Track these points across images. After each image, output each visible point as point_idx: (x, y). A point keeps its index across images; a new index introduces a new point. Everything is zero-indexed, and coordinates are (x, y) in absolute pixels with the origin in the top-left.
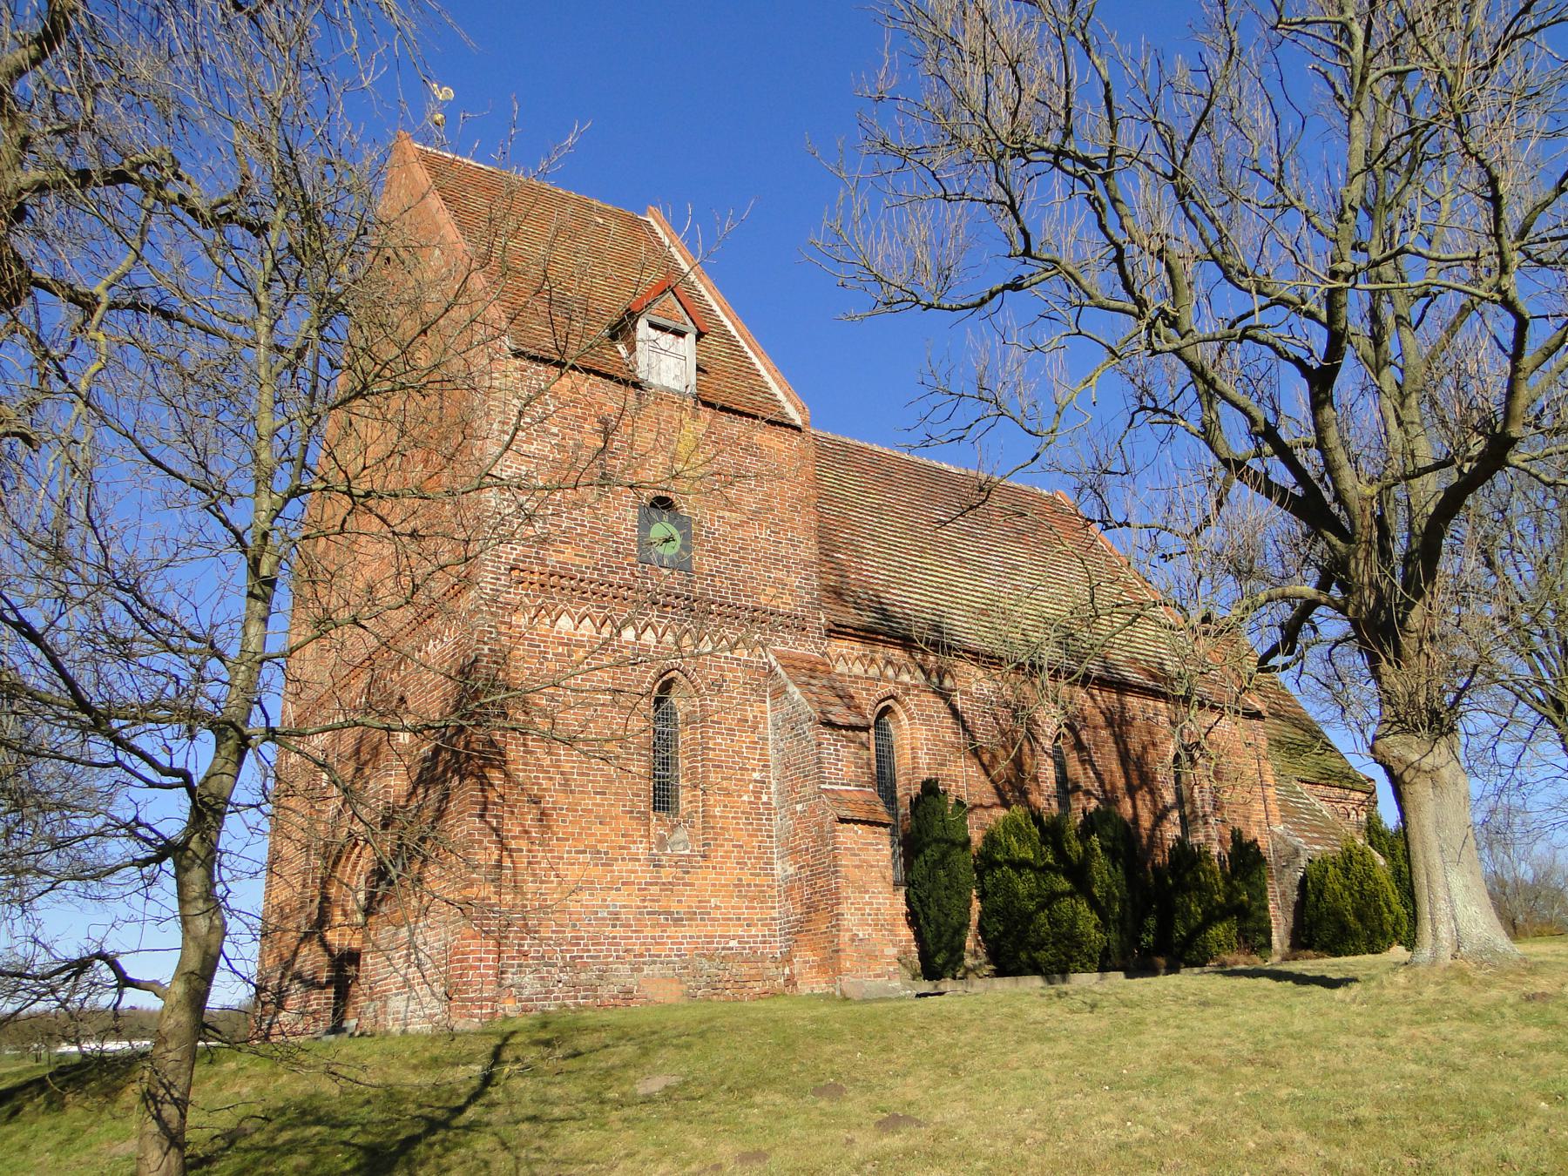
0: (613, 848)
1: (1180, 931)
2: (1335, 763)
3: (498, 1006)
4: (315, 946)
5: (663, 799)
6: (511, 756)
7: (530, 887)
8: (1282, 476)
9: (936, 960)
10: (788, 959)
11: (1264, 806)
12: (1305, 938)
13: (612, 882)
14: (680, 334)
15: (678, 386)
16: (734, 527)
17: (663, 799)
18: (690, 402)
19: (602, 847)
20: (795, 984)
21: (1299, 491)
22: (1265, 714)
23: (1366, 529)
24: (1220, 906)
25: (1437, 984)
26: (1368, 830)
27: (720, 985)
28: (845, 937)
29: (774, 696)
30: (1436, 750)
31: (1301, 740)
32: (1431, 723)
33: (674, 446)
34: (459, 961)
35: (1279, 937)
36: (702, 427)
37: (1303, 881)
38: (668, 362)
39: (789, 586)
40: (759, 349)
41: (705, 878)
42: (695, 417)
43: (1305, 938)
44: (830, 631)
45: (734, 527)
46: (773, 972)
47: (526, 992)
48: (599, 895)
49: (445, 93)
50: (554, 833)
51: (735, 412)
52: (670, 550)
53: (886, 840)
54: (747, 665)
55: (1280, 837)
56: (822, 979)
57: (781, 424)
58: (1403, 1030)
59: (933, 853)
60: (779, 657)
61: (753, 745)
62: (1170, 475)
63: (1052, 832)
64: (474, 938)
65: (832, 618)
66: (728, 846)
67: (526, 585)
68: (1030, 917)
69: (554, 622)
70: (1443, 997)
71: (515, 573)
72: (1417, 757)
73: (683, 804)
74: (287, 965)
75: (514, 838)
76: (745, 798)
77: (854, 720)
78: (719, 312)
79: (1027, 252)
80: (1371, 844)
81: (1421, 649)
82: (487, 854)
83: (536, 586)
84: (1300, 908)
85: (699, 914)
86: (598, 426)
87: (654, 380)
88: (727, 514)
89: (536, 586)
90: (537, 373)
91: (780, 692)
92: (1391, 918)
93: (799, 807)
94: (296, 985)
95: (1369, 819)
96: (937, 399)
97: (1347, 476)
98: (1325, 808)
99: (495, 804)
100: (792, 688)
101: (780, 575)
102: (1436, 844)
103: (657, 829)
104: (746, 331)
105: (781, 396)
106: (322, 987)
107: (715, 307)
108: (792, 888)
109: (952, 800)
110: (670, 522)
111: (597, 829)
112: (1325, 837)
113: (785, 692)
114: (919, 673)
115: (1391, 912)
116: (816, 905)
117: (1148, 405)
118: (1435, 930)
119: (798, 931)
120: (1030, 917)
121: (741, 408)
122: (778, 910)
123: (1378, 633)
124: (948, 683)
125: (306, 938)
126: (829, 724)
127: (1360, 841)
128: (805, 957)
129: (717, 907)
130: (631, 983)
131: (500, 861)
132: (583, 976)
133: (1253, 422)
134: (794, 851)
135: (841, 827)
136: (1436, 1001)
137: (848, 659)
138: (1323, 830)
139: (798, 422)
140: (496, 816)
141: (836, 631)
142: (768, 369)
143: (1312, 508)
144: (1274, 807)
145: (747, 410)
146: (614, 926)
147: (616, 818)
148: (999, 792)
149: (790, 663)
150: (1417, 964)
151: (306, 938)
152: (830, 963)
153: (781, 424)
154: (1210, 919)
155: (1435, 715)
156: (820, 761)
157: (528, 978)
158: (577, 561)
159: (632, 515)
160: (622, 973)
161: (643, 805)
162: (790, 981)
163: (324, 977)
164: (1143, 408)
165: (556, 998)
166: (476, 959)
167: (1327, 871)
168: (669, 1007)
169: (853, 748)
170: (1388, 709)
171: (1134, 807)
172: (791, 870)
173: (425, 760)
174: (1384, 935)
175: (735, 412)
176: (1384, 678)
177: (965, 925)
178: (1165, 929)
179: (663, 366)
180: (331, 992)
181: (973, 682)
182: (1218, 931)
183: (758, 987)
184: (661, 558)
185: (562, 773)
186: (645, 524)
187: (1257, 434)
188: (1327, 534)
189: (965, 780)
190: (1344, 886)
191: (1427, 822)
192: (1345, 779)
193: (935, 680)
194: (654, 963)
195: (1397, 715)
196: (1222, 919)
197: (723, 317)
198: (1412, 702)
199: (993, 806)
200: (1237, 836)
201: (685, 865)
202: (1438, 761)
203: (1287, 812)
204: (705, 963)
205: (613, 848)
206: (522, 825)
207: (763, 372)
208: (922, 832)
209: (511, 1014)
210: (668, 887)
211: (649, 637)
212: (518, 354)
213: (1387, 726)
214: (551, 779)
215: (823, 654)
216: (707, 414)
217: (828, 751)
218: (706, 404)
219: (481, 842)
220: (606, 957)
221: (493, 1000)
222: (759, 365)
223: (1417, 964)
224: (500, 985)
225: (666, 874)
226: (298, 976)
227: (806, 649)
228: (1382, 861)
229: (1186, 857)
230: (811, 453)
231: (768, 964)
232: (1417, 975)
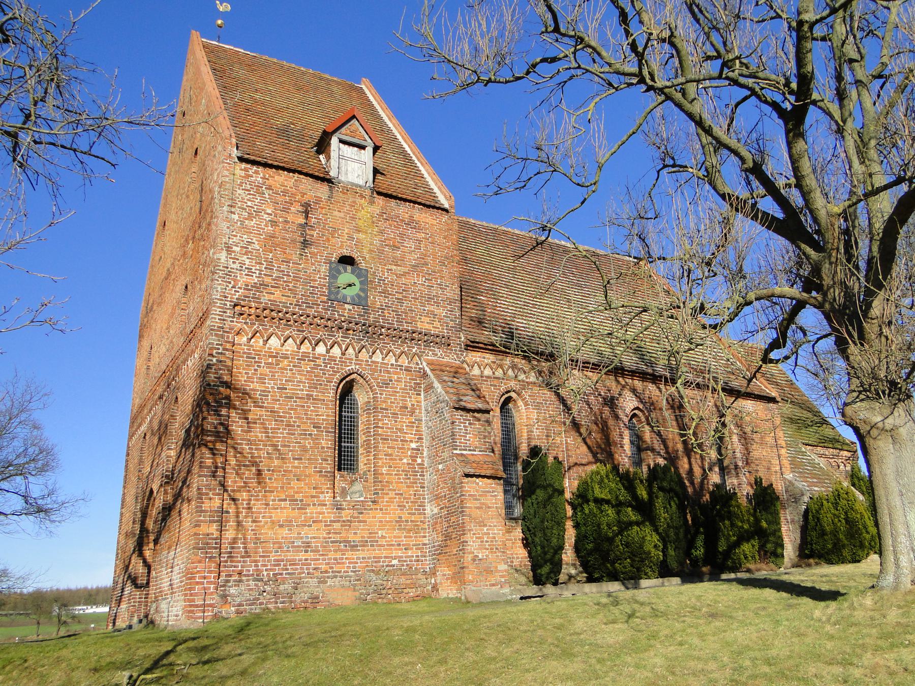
0: (307, 497)
1: (722, 546)
2: (827, 432)
5: (345, 460)
8: (769, 205)
9: (543, 569)
10: (433, 573)
11: (783, 461)
12: (810, 552)
13: (306, 521)
14: (363, 147)
15: (361, 182)
17: (345, 460)
18: (368, 192)
19: (299, 497)
20: (437, 590)
21: (780, 215)
22: (779, 399)
23: (834, 237)
24: (746, 531)
25: (899, 607)
26: (852, 476)
27: (383, 592)
28: (469, 557)
29: (426, 391)
30: (896, 414)
31: (806, 421)
32: (891, 391)
33: (356, 226)
35: (790, 550)
36: (376, 209)
37: (807, 512)
38: (352, 166)
39: (438, 316)
40: (424, 161)
41: (374, 517)
42: (372, 202)
43: (810, 552)
44: (467, 346)
46: (424, 581)
49: (224, 7)
51: (401, 199)
52: (354, 291)
53: (500, 489)
54: (408, 370)
55: (790, 482)
56: (455, 587)
57: (434, 207)
58: (868, 659)
59: (540, 494)
60: (430, 364)
61: (411, 425)
62: (690, 219)
63: (628, 481)
64: (200, 562)
65: (469, 337)
66: (392, 494)
68: (611, 540)
70: (904, 621)
72: (879, 419)
73: (361, 466)
76: (405, 461)
77: (480, 405)
78: (401, 140)
79: (557, 30)
80: (854, 485)
81: (881, 334)
83: (253, 317)
84: (804, 530)
85: (370, 542)
87: (342, 178)
88: (394, 267)
89: (253, 317)
90: (256, 172)
91: (430, 387)
92: (868, 537)
93: (440, 467)
95: (853, 468)
96: (508, 162)
97: (819, 202)
98: (822, 462)
100: (437, 384)
101: (432, 308)
102: (896, 490)
103: (340, 483)
104: (417, 150)
105: (436, 190)
107: (399, 137)
108: (436, 523)
109: (550, 459)
110: (353, 272)
111: (295, 484)
112: (821, 482)
113: (433, 387)
115: (868, 532)
116: (452, 533)
117: (670, 163)
118: (897, 560)
119: (440, 552)
120: (611, 540)
121: (404, 196)
122: (431, 538)
123: (848, 320)
126: (464, 409)
127: (846, 484)
128: (444, 571)
130: (317, 591)
132: (282, 587)
133: (743, 160)
134: (437, 497)
135: (466, 480)
136: (898, 624)
137: (481, 365)
138: (820, 476)
139: (446, 206)
141: (472, 346)
142: (429, 173)
143: (791, 225)
144: (785, 462)
145: (409, 198)
147: (310, 476)
148: (595, 455)
149: (438, 369)
150: (882, 588)
152: (459, 577)
153: (434, 207)
154: (744, 537)
155: (893, 384)
158: (284, 299)
159: (324, 268)
160: (311, 585)
161: (329, 466)
162: (435, 588)
164: (665, 166)
166: (200, 578)
167: (822, 505)
168: (342, 609)
169: (478, 425)
170: (856, 382)
171: (690, 463)
172: (436, 511)
174: (862, 546)
175: (401, 199)
176: (851, 358)
177: (561, 548)
178: (711, 544)
179: (349, 169)
181: (576, 382)
182: (746, 547)
183: (412, 593)
184: (345, 297)
186: (333, 275)
187: (746, 170)
188: (803, 246)
189: (567, 448)
190: (834, 515)
191: (889, 472)
192: (835, 442)
194: (336, 577)
195: (862, 384)
196: (748, 541)
197: (403, 143)
198: (875, 377)
199: (589, 463)
200: (758, 482)
201: (360, 508)
202: (898, 422)
203: (795, 465)
205: (307, 497)
207: (426, 175)
208: (528, 481)
210: (348, 524)
211: (341, 355)
212: (241, 159)
213: (855, 394)
215: (463, 362)
216: (380, 200)
217: (460, 428)
218: (379, 193)
219: (207, 494)
220: (300, 573)
222: (423, 171)
223: (882, 588)
225: (346, 514)
227: (450, 358)
228: (861, 497)
229: (723, 497)
230: (456, 227)
231: (420, 576)
232: (882, 598)
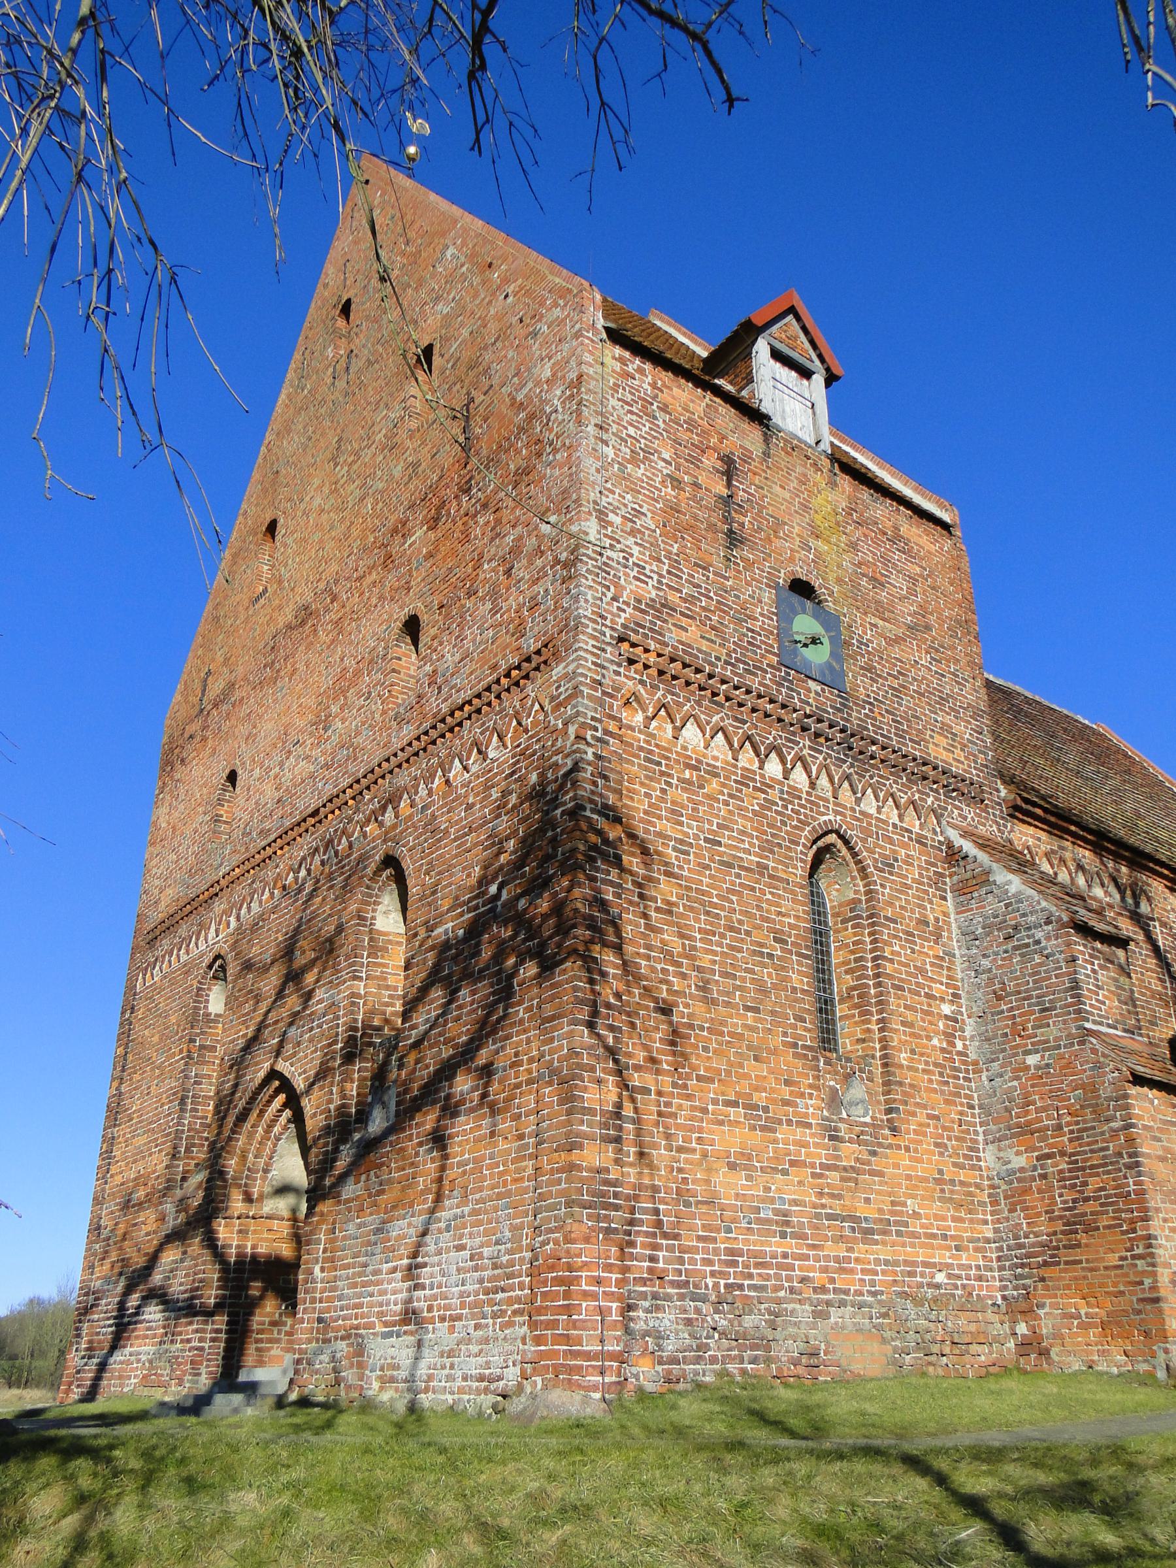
3: (628, 1371)
4: (195, 1245)
6: (628, 931)
7: (660, 1154)
16: (891, 642)
19: (760, 1098)
20: (1044, 1353)
27: (935, 1349)
34: (559, 1281)
41: (897, 1164)
42: (833, 484)
44: (1016, 808)
45: (891, 642)
47: (670, 1346)
48: (762, 1178)
50: (693, 1068)
52: (818, 656)
67: (640, 666)
69: (678, 730)
71: (625, 646)
74: (138, 1278)
75: (637, 1068)
76: (935, 1042)
82: (599, 1094)
86: (719, 465)
89: (653, 672)
90: (640, 371)
93: (1032, 1060)
94: (153, 1313)
99: (608, 1006)
101: (948, 719)
106: (209, 1314)
108: (1026, 1191)
114: (1112, 889)
119: (1038, 1267)
124: (1144, 908)
125: (176, 1236)
129: (916, 1215)
131: (619, 1105)
134: (1026, 1131)
135: (1134, 1090)
140: (612, 1028)
141: (1020, 812)
146: (783, 1235)
147: (775, 1052)
151: (176, 1236)
156: (1075, 985)
157: (667, 1320)
163: (211, 1297)
165: (713, 1359)
172: (1020, 1161)
173: (446, 946)
180: (221, 1321)
185: (699, 969)
186: (785, 616)
193: (1130, 901)
204: (911, 1310)
206: (646, 1048)
209: (650, 1387)
210: (851, 1174)
214: (684, 976)
219: (592, 1069)
220: (777, 1289)
221: (621, 1358)
224: (627, 1331)
226: (158, 1295)
